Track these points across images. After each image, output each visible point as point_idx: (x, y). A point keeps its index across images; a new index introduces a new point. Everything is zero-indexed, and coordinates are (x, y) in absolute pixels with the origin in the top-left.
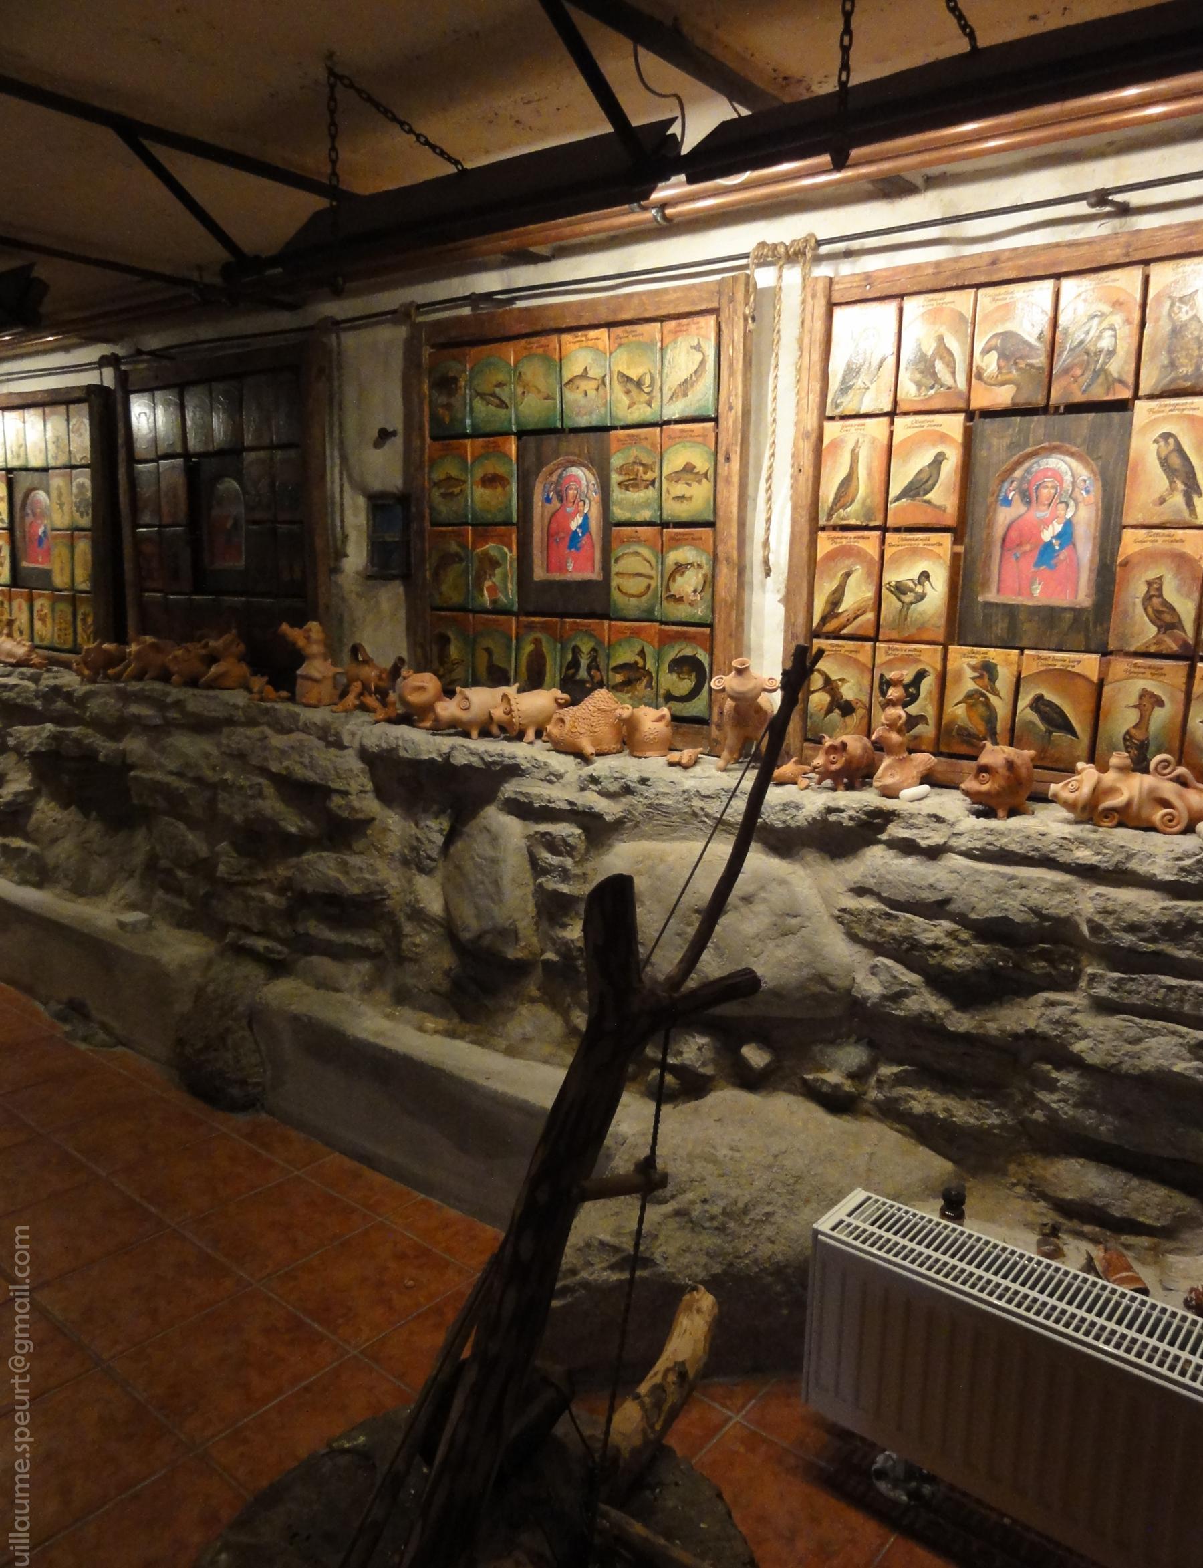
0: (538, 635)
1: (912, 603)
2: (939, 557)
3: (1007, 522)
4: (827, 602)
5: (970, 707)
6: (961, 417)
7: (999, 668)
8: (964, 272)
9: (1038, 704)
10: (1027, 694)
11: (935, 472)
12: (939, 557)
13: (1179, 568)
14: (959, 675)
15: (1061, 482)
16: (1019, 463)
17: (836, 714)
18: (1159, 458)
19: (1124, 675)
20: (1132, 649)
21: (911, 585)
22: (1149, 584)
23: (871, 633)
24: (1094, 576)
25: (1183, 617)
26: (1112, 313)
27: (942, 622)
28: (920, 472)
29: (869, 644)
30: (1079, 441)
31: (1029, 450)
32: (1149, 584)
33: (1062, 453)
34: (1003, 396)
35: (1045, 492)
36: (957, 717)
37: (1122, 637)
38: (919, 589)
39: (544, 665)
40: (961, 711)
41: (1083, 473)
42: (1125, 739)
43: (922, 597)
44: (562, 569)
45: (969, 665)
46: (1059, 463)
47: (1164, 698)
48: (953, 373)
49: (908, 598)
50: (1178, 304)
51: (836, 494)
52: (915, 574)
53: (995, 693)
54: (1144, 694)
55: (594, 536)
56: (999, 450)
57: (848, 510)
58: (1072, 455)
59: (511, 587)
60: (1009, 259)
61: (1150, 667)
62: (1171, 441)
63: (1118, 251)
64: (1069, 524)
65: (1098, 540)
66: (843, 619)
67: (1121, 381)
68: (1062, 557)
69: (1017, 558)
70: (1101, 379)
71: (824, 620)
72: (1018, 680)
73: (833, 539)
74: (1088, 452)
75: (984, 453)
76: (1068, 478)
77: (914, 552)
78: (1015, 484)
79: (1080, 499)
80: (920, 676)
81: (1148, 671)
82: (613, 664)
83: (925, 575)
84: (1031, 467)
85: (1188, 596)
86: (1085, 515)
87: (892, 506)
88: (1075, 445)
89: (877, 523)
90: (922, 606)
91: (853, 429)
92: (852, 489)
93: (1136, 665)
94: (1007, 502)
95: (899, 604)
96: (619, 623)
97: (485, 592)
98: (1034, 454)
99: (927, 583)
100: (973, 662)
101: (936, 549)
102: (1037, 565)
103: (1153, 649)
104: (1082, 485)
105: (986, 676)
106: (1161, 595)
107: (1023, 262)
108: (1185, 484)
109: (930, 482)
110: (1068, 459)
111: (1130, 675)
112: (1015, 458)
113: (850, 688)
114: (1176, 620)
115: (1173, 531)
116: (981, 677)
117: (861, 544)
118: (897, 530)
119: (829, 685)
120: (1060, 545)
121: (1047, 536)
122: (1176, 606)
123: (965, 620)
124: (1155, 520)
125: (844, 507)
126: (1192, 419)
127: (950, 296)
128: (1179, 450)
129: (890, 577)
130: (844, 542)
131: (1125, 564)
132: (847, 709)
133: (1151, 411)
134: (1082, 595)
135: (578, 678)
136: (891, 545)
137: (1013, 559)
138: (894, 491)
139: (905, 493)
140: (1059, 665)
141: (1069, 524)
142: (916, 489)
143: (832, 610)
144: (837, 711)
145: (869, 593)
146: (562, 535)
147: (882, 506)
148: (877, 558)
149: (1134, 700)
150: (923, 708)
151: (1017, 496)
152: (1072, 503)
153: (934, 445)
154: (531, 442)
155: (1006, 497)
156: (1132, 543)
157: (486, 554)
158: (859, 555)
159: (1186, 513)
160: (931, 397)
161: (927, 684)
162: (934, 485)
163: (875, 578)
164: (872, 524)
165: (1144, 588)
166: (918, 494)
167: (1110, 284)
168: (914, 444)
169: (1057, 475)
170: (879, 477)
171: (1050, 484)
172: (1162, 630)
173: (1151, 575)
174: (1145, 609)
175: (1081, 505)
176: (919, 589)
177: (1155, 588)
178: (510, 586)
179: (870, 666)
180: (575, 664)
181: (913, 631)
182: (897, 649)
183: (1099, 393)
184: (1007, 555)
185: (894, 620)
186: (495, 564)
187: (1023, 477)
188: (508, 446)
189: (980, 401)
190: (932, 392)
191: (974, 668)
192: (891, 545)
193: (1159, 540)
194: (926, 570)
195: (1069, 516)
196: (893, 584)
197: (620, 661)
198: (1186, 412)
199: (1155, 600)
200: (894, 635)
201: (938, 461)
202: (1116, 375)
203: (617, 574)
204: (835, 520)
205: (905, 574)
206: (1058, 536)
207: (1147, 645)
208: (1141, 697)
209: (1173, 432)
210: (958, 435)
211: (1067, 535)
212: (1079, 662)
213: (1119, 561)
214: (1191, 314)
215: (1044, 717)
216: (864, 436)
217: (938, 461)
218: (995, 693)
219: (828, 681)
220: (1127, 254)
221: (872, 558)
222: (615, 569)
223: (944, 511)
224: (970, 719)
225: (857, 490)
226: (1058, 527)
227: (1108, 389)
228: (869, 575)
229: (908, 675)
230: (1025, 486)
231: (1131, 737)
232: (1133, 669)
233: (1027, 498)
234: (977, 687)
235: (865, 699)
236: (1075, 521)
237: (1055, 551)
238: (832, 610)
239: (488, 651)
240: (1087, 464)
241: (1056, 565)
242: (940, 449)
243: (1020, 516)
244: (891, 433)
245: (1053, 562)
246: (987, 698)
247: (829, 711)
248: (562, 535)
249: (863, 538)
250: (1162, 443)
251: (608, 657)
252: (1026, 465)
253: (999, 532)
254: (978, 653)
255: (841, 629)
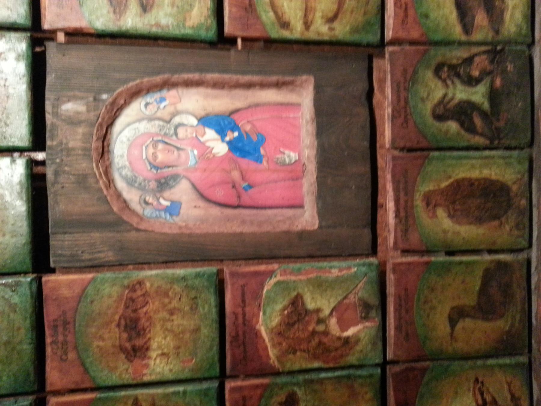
0: (419, 202)
3: (201, 203)
39: (471, 182)
44: (295, 173)
55: (238, 104)
59: (335, 269)
64: (205, 120)
68: (248, 127)
69: (250, 186)
78: (150, 199)
79: (171, 109)
82: (457, 32)
96: (390, 21)
97: (350, 332)
98: (107, 172)
102: (259, 159)
120: (233, 130)
121: (221, 148)
135: (486, 106)
141: (205, 120)
146: (236, 175)
151: (167, 194)
154: (60, 244)
155: (167, 210)
157: (279, 333)
175: (180, 107)
178: (335, 272)
180: (463, 113)
184: (246, 199)
186: (297, 312)
187: (141, 188)
188: (66, 292)
195: (195, 122)
197: (453, 16)
203: (307, 25)
206: (222, 133)
211: (221, 123)
222: (297, 31)
236: (203, 113)
239: (457, 315)
241: (258, 134)
245: (254, 138)
248: (236, 175)
251: (448, 43)
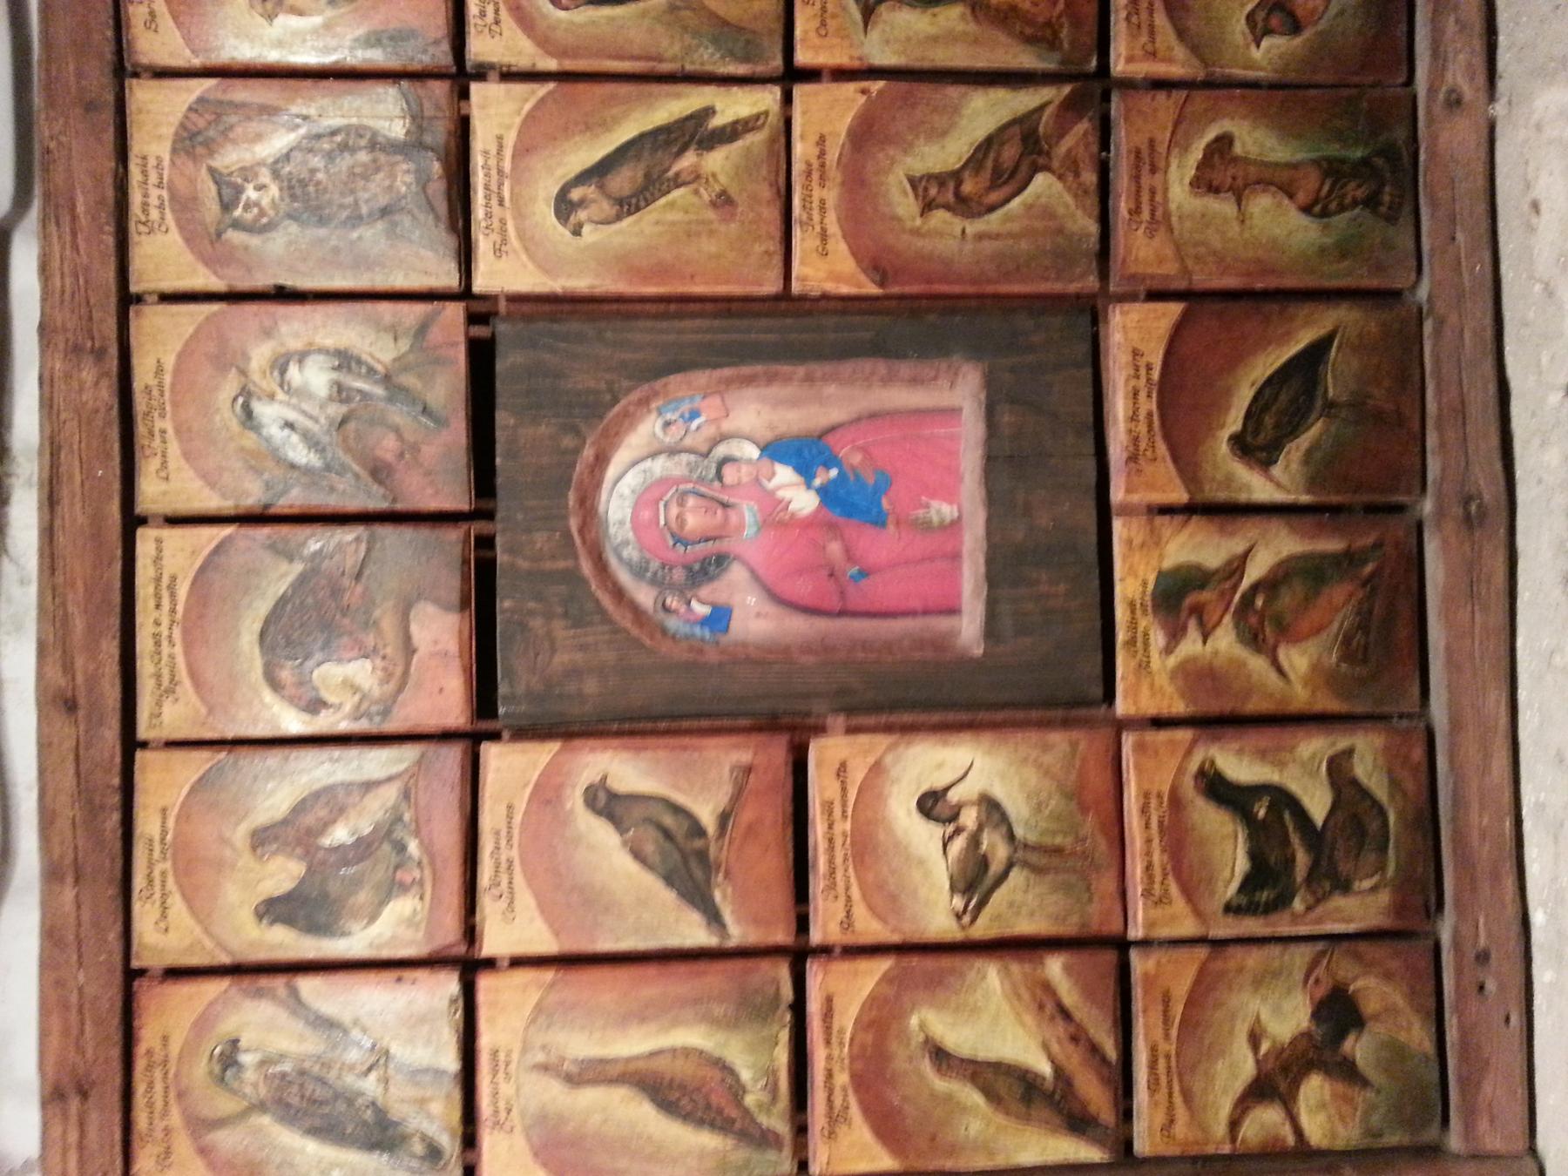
1: (1011, 836)
2: (877, 769)
3: (770, 608)
4: (1026, 1119)
5: (1286, 631)
6: (492, 754)
7: (1168, 564)
8: (84, 789)
9: (1256, 446)
10: (1229, 479)
11: (638, 812)
12: (877, 769)
13: (888, 140)
14: (1196, 676)
15: (665, 482)
16: (619, 593)
17: (1359, 1048)
18: (618, 218)
19: (1161, 235)
20: (1093, 228)
21: (958, 844)
22: (928, 207)
23: (1109, 957)
24: (905, 368)
25: (1005, 115)
26: (243, 373)
27: (1059, 739)
28: (638, 855)
29: (1140, 964)
30: (568, 441)
31: (586, 568)
32: (928, 207)
33: (598, 485)
34: (440, 631)
35: (694, 522)
36: (1315, 668)
37: (1063, 258)
38: (969, 818)
40: (1297, 659)
41: (648, 430)
42: (1325, 214)
43: (991, 807)
45: (1168, 650)
46: (620, 499)
47: (1211, 134)
48: (369, 786)
49: (996, 848)
50: (238, 212)
51: (700, 1123)
52: (923, 837)
53: (1236, 567)
54: (1204, 183)
56: (583, 648)
57: (746, 1075)
58: (601, 460)
60: (68, 668)
61: (1136, 178)
62: (575, 194)
63: (88, 374)
64: (775, 450)
65: (818, 369)
66: (1074, 1060)
67: (422, 329)
69: (865, 573)
70: (409, 380)
71: (1078, 1123)
72: (1191, 510)
73: (836, 1119)
74: (594, 416)
75: (591, 686)
76: (659, 467)
77: (866, 846)
78: (673, 602)
79: (710, 431)
80: (1216, 787)
81: (1146, 181)
83: (931, 804)
84: (629, 564)
85: (956, 110)
86: (751, 414)
87: (738, 933)
88: (577, 451)
89: (784, 972)
90: (1017, 808)
91: (506, 1089)
92: (683, 1070)
93: (1135, 211)
94: (720, 617)
95: (1017, 877)
98: (601, 566)
99: (954, 796)
100: (1158, 639)
101: (857, 775)
102: (879, 522)
103: (1090, 177)
104: (676, 433)
105: (1189, 601)
106: (957, 176)
107: (79, 624)
108: (683, 149)
109: (668, 820)
110: (611, 472)
111: (1160, 221)
112: (607, 601)
113: (1277, 1010)
114: (1016, 129)
115: (797, 167)
116: (1198, 611)
117: (847, 1018)
118: (803, 924)
119: (1274, 1085)
120: (827, 467)
121: (804, 502)
122: (980, 134)
123: (1047, 678)
124: (772, 214)
125: (737, 1091)
126: (524, 150)
127: (147, 825)
128: (599, 172)
129: (937, 912)
130: (842, 1078)
131: (877, 267)
132: (1338, 1013)
133: (498, 252)
134: (953, 403)
136: (848, 923)
137: (864, 583)
138: (693, 932)
139: (699, 898)
140: (1149, 405)
141: (775, 450)
142: (687, 862)
143: (1049, 1097)
144: (1348, 1044)
145: (991, 977)
147: (737, 965)
148: (884, 965)
149: (1223, 207)
150: (1309, 770)
151: (704, 592)
152: (721, 450)
153: (564, 820)
155: (704, 622)
156: (826, 266)
158: (881, 1019)
159: (755, 139)
160: (427, 847)
161: (1240, 767)
162: (677, 810)
163: (946, 962)
164: (787, 993)
165: (940, 217)
166: (702, 855)
167: (168, 379)
168: (562, 890)
169: (650, 496)
170: (653, 985)
171: (674, 511)
172: (1041, 161)
173: (905, 205)
174: (992, 209)
175: (727, 426)
176: (969, 818)
177: (937, 191)
179: (1202, 952)
181: (1089, 824)
182: (1149, 867)
183: (447, 387)
184: (855, 600)
185: (1067, 888)
187: (654, 582)
189: (444, 698)
190: (413, 847)
191: (1175, 635)
192: (848, 923)
193: (821, 204)
194: (920, 808)
195: (752, 452)
196: (958, 902)
198: (507, 165)
199: (968, 187)
200: (1108, 883)
201: (608, 803)
202: (404, 345)
204: (778, 1122)
205: (928, 855)
206: (805, 472)
207: (1079, 193)
208: (1214, 190)
209: (555, 190)
210: (542, 754)
211: (801, 452)
212: (1136, 353)
213: (873, 290)
214: (265, 177)
215: (1291, 427)
216: (525, 1049)
217: (608, 803)
218: (1236, 567)
219: (1260, 1090)
220: (99, 354)
221: (886, 979)
223: (749, 770)
224: (1318, 631)
225: (687, 1052)
226: (784, 475)
227: (438, 361)
228: (934, 983)
229: (1213, 821)
230: (679, 575)
231: (1316, 201)
232: (1146, 215)
233: (708, 568)
234: (1228, 619)
235: (1300, 956)
236: (768, 436)
237: (842, 476)
238: (1049, 1097)
240: (628, 420)
242: (575, 800)
243: (752, 571)
244: (518, 962)
246: (1255, 588)
247: (1348, 1072)
249: (828, 1014)
250: (582, 215)
252: (624, 577)
253: (798, 627)
254: (1133, 625)
255: (1104, 1060)
